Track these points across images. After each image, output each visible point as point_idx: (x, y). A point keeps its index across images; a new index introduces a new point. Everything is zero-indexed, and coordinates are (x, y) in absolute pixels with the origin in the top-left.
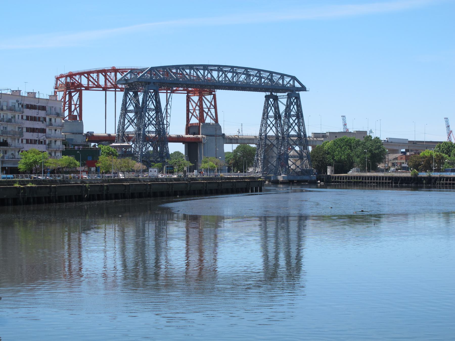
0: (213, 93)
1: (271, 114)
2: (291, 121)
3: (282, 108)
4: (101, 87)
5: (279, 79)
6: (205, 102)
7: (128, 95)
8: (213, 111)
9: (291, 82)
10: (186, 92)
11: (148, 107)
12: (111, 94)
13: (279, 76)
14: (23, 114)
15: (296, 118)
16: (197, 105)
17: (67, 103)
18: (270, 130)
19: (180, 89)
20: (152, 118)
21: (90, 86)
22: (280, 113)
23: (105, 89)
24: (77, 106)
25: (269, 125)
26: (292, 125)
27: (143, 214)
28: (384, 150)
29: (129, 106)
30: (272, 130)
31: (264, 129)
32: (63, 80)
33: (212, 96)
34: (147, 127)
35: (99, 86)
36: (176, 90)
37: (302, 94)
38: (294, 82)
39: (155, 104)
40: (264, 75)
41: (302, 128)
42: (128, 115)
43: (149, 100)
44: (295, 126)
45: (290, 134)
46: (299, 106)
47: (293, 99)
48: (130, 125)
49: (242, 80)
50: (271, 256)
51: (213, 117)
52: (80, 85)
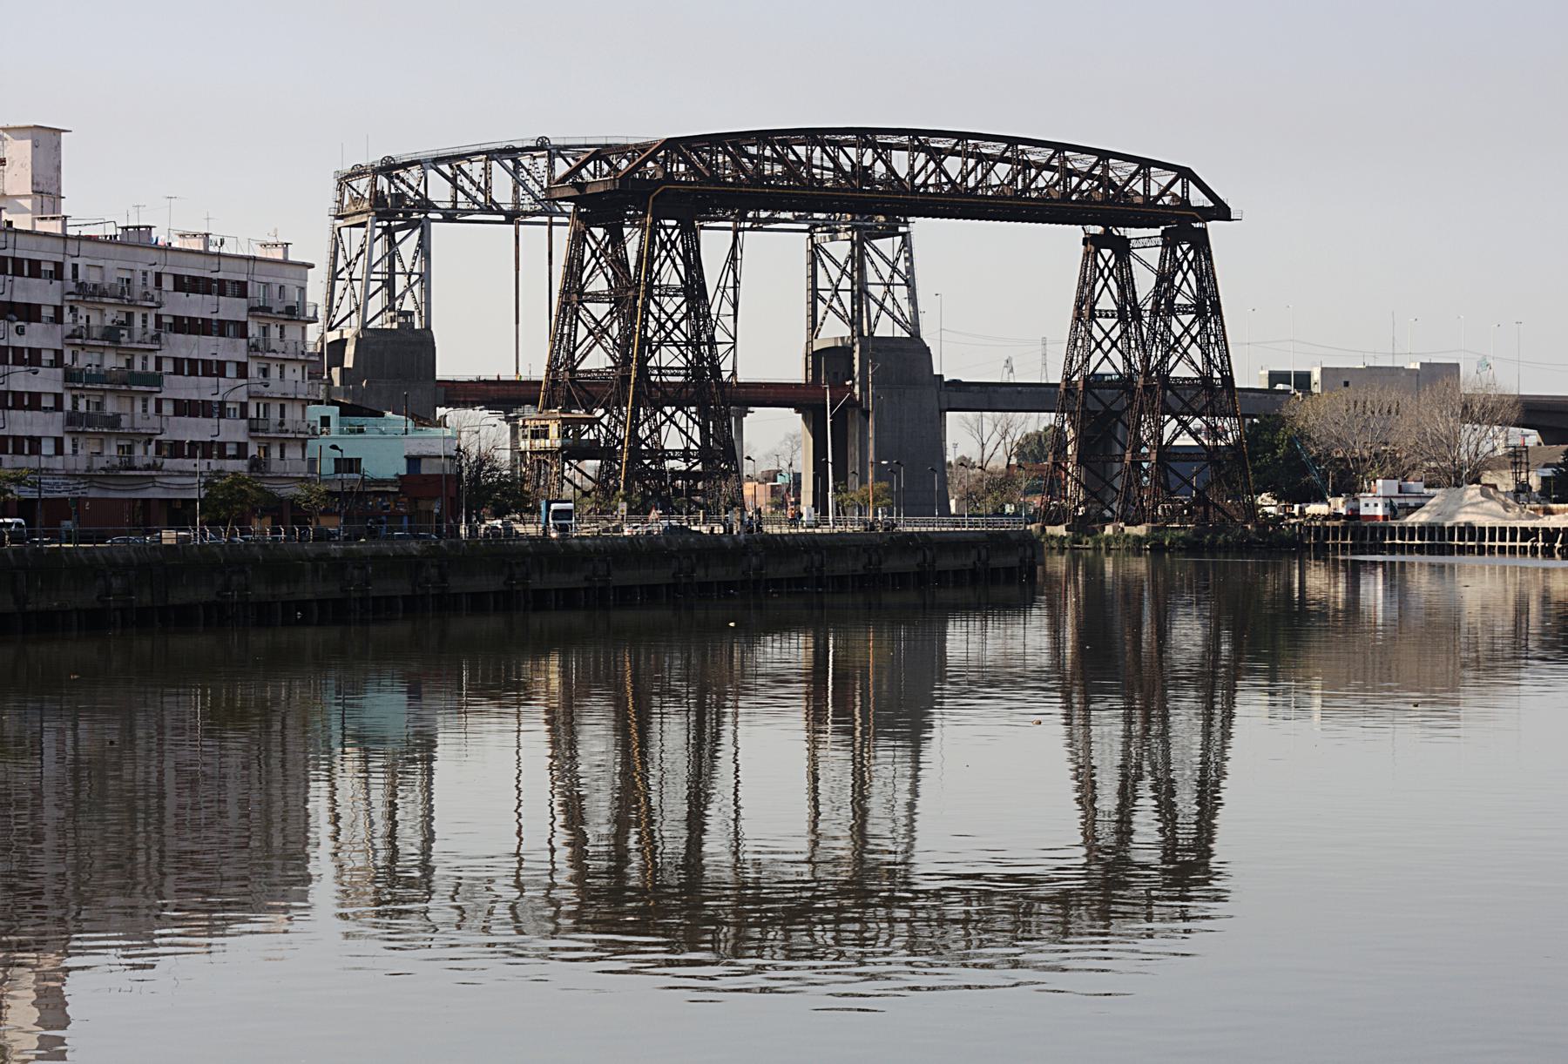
0: (902, 229)
1: (1106, 303)
2: (1177, 329)
3: (1145, 284)
4: (500, 212)
5: (1132, 177)
6: (872, 262)
7: (588, 237)
8: (901, 292)
10: (806, 227)
11: (656, 283)
12: (533, 235)
13: (1134, 167)
14: (161, 311)
15: (1194, 319)
16: (844, 271)
17: (378, 269)
18: (1102, 360)
19: (783, 215)
20: (673, 321)
21: (459, 206)
22: (1139, 301)
23: (513, 217)
24: (414, 278)
25: (1099, 345)
26: (1180, 344)
27: (332, 683)
29: (591, 280)
31: (1080, 358)
32: (362, 184)
33: (899, 239)
34: (653, 353)
35: (491, 207)
36: (768, 220)
37: (1214, 227)
38: (1185, 187)
39: (681, 269)
40: (1077, 165)
41: (1217, 355)
42: (588, 312)
43: (659, 256)
44: (1189, 346)
45: (1172, 375)
46: (1206, 277)
47: (1181, 249)
48: (594, 344)
49: (999, 182)
50: (1108, 801)
52: (426, 205)
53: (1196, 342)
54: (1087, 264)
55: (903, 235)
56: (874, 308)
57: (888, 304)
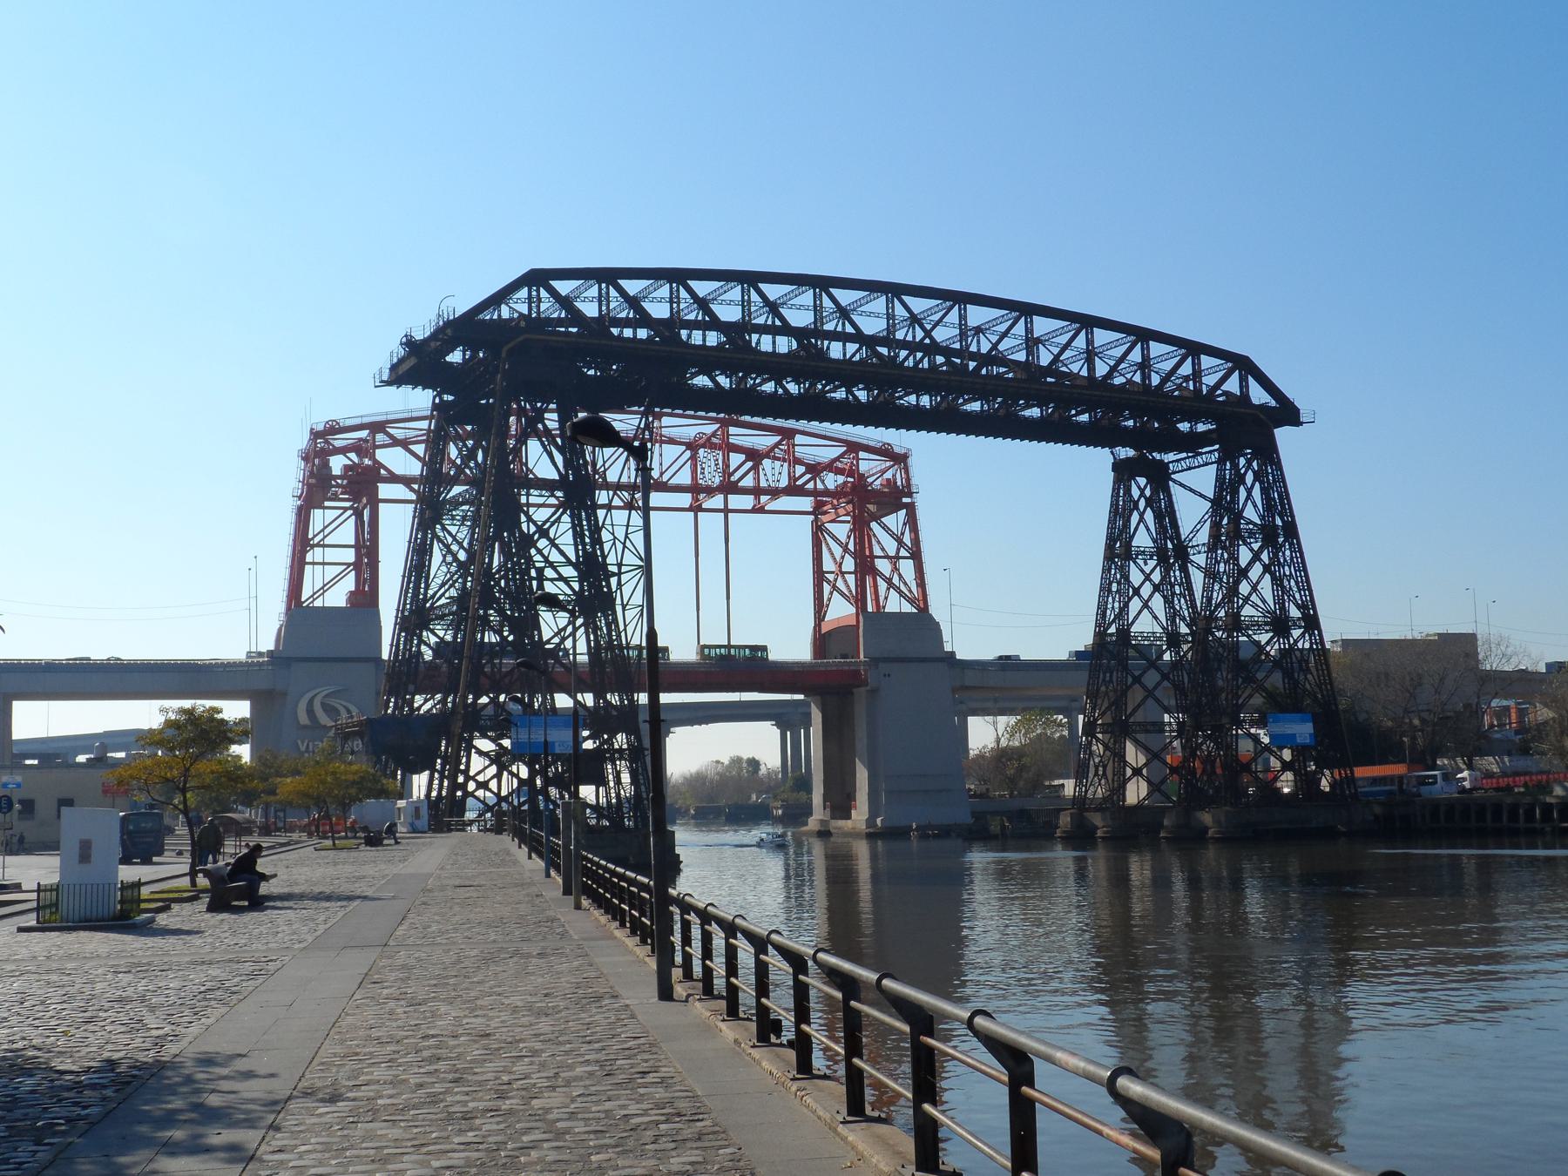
0: (905, 500)
1: (1142, 540)
3: (1192, 513)
8: (907, 567)
22: (1183, 537)
25: (1137, 592)
30: (1152, 613)
31: (1117, 605)
37: (1283, 435)
41: (1184, 607)
44: (1151, 596)
46: (1278, 503)
51: (910, 591)
53: (1134, 588)
55: (906, 506)
56: (882, 586)
57: (896, 580)
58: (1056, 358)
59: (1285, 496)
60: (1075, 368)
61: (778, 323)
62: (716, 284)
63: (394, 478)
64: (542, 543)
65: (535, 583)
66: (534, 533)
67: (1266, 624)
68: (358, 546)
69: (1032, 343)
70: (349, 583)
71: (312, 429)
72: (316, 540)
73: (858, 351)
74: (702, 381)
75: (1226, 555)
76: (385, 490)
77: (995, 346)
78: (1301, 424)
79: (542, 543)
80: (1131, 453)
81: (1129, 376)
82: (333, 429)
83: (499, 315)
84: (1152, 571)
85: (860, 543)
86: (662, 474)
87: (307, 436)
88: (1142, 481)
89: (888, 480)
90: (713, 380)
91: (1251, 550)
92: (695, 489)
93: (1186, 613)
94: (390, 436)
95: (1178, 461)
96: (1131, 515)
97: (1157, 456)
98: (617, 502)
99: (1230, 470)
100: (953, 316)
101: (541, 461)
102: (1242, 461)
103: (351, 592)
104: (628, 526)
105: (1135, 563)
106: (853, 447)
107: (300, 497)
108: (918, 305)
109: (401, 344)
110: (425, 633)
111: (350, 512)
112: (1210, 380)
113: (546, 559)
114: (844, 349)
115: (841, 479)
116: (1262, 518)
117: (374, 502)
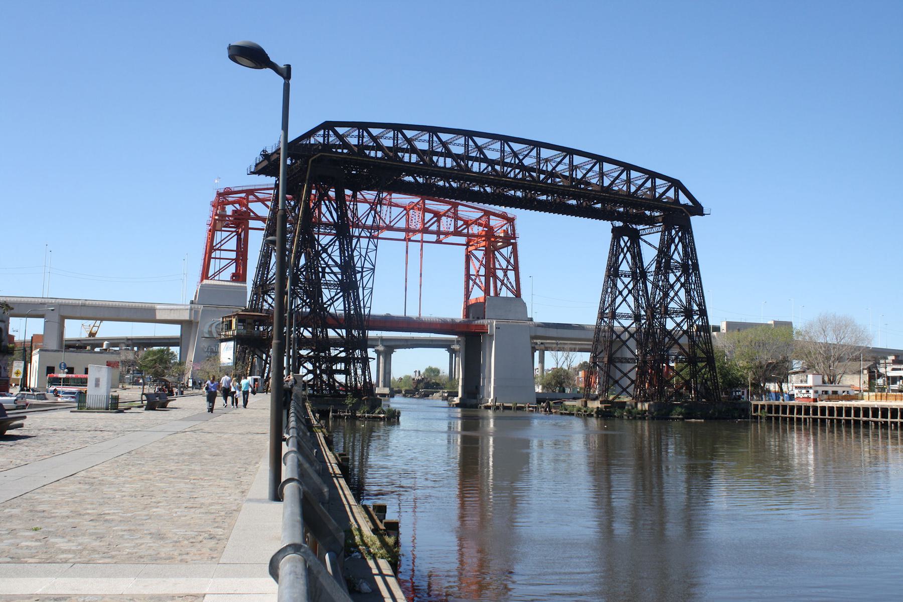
0: (512, 241)
1: (625, 267)
3: (649, 255)
8: (511, 274)
9: (671, 194)
22: (645, 267)
25: (621, 293)
28: (598, 407)
31: (610, 299)
37: (695, 220)
41: (644, 302)
44: (627, 295)
46: (690, 252)
51: (512, 287)
54: (614, 244)
56: (499, 284)
57: (505, 281)
58: (585, 175)
59: (694, 250)
60: (594, 181)
61: (482, 156)
62: (452, 136)
63: (257, 218)
64: (324, 255)
65: (321, 274)
66: (321, 250)
67: (682, 312)
68: (238, 251)
69: (573, 168)
70: (232, 269)
71: (218, 192)
72: (217, 247)
73: (486, 168)
74: (409, 179)
75: (663, 277)
76: (252, 224)
77: (554, 168)
78: (704, 215)
79: (324, 255)
80: (621, 224)
81: (620, 187)
82: (228, 192)
83: (310, 142)
84: (629, 283)
85: (488, 262)
86: (390, 222)
87: (215, 195)
88: (626, 238)
89: (504, 230)
90: (414, 178)
91: (676, 276)
92: (407, 230)
93: (644, 305)
94: (256, 197)
95: (644, 229)
96: (620, 255)
97: (634, 226)
98: (363, 234)
99: (668, 235)
100: (534, 153)
101: (327, 214)
102: (673, 232)
103: (233, 273)
104: (367, 249)
105: (620, 278)
106: (487, 213)
107: (210, 225)
108: (516, 147)
109: (261, 155)
110: (265, 296)
111: (235, 233)
112: (660, 191)
113: (326, 263)
114: (480, 166)
115: (481, 228)
116: (682, 260)
117: (247, 229)
